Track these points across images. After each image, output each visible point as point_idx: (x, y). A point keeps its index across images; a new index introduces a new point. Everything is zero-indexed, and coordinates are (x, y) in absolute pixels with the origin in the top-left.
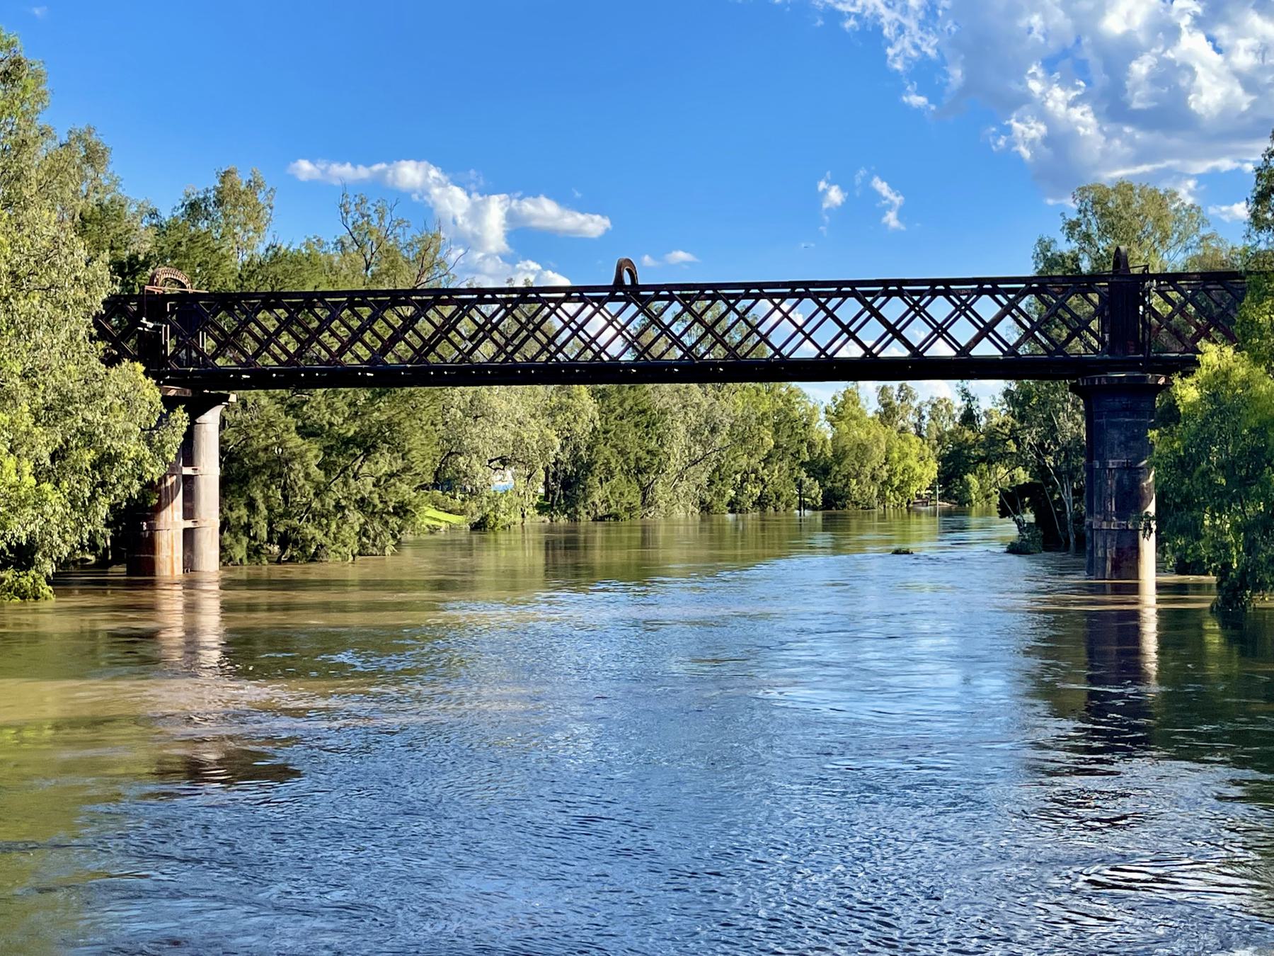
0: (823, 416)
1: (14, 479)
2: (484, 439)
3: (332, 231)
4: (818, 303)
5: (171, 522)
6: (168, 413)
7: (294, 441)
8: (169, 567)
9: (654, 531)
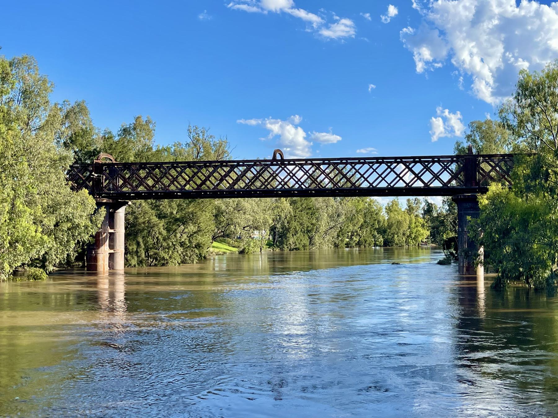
0: (384, 210)
1: (34, 234)
2: (241, 219)
3: (185, 139)
5: (104, 251)
6: (98, 209)
7: (155, 219)
8: (103, 267)
9: (314, 255)
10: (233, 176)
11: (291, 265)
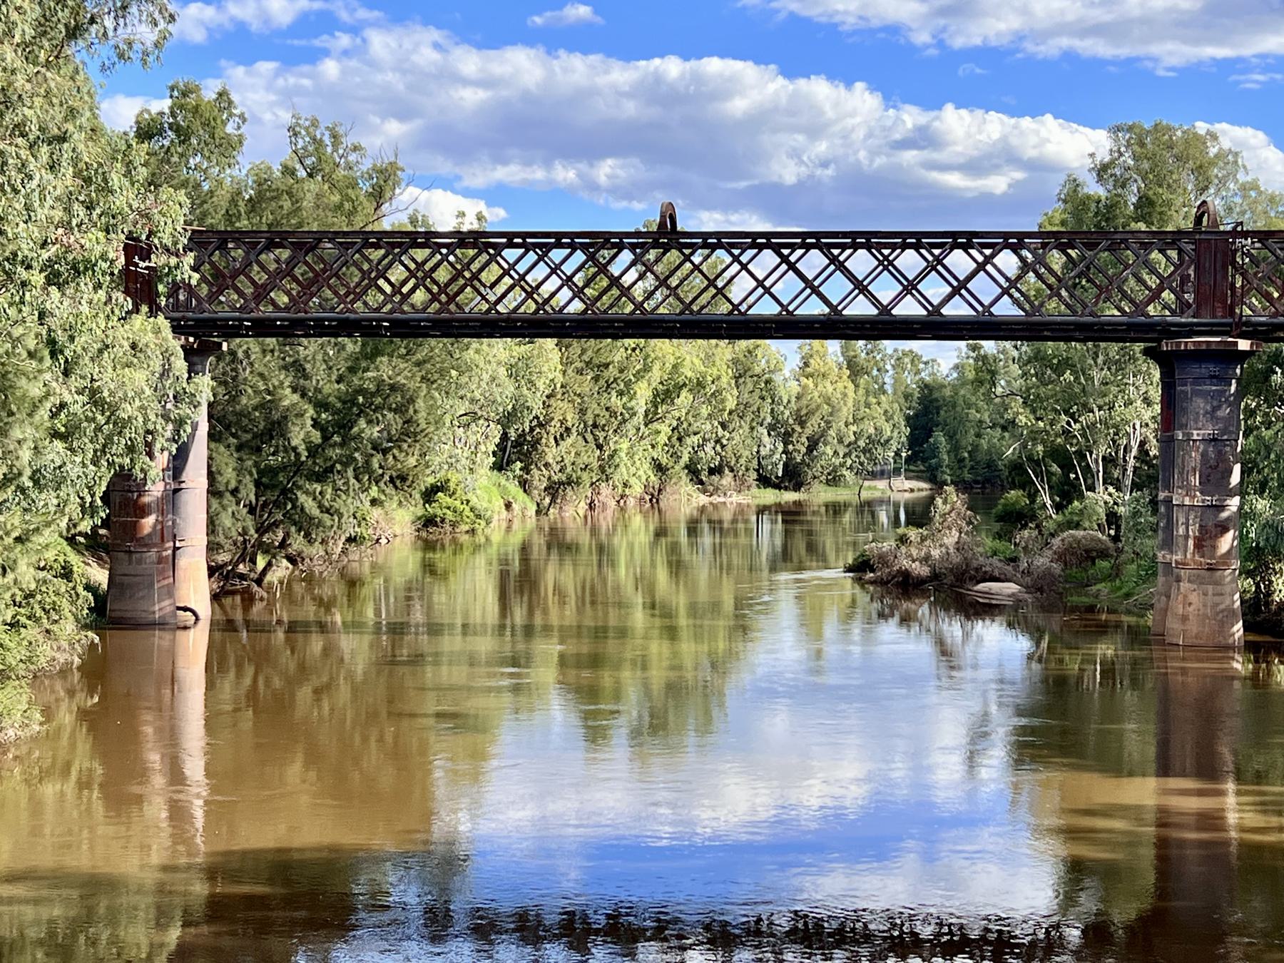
4: (732, 254)
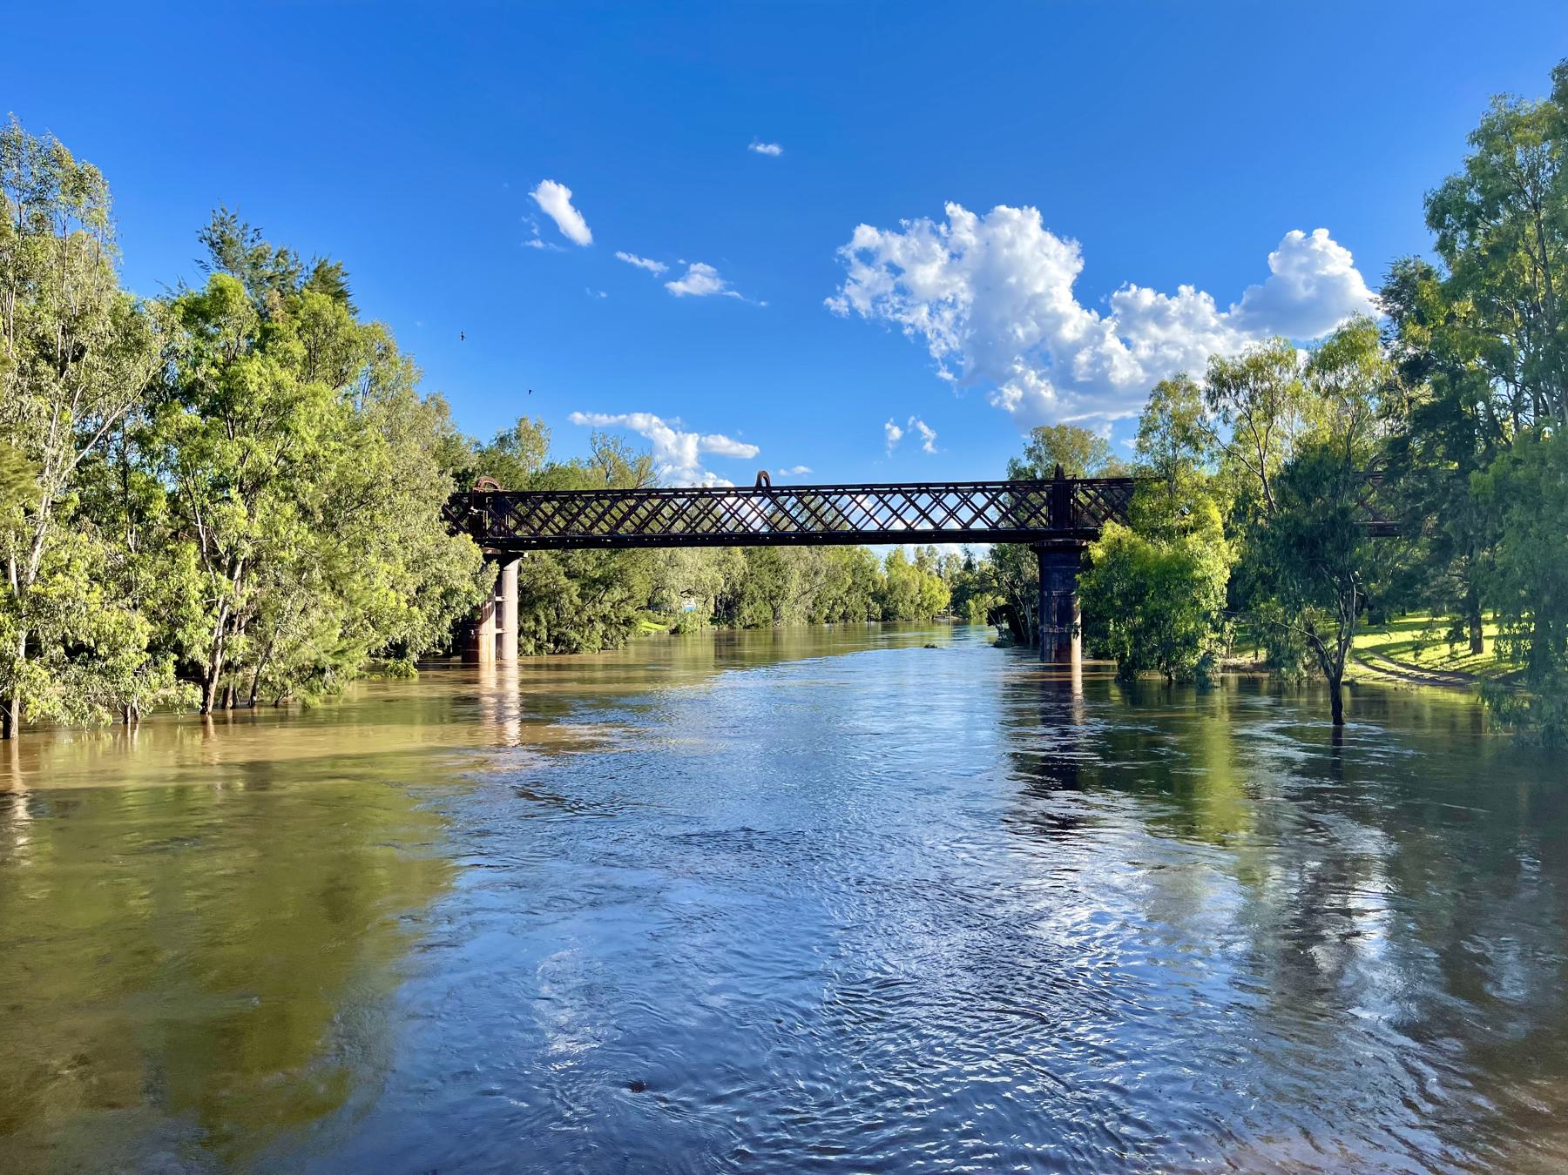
5: (488, 631)
7: (563, 581)
10: (642, 512)
11: (747, 650)
